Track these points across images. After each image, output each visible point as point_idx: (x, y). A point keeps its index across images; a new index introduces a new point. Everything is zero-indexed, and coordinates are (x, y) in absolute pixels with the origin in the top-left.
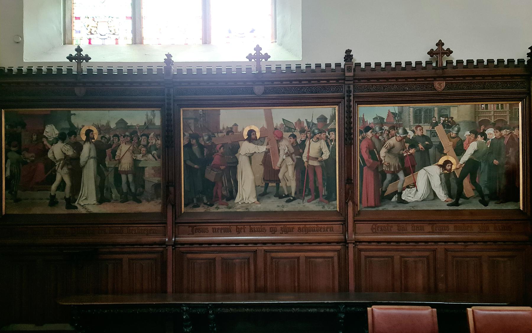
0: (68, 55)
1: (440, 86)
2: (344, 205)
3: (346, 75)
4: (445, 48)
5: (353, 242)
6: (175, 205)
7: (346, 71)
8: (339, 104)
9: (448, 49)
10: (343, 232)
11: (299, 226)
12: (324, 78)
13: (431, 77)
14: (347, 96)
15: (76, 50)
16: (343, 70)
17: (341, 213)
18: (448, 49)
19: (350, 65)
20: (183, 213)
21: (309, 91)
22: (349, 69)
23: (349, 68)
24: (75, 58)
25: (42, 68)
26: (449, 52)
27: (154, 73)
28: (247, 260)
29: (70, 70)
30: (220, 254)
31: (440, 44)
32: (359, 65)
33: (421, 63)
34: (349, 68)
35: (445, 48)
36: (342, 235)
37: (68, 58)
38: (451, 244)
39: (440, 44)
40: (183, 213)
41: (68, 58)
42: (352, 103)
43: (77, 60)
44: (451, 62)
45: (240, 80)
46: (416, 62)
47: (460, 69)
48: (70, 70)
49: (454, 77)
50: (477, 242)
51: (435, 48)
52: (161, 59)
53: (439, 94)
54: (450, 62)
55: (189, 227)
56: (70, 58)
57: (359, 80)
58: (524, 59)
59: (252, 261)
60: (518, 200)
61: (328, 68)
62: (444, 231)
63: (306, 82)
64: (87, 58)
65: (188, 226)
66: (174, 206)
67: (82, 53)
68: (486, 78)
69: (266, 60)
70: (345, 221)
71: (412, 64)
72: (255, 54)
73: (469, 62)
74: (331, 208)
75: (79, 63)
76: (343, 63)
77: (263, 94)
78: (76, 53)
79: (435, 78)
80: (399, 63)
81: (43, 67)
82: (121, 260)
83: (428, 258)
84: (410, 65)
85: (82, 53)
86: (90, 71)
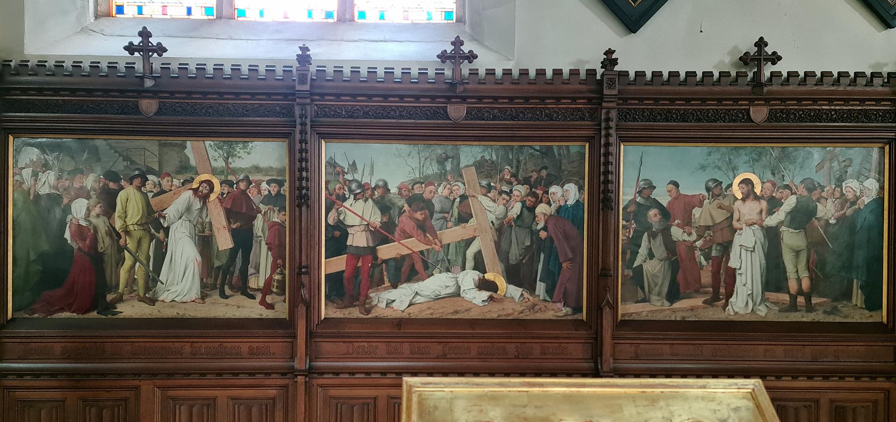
0: (127, 44)
1: (457, 111)
2: (596, 309)
3: (605, 93)
4: (769, 50)
5: (305, 373)
6: (310, 306)
7: (605, 85)
8: (892, 142)
9: (774, 53)
10: (592, 357)
11: (250, 344)
12: (711, 97)
13: (536, 98)
14: (300, 124)
15: (140, 34)
16: (601, 82)
17: (590, 324)
18: (774, 53)
19: (305, 72)
20: (322, 319)
21: (630, 115)
22: (303, 79)
23: (303, 77)
24: (138, 49)
25: (46, 64)
26: (775, 58)
27: (190, 76)
28: (272, 401)
29: (130, 67)
30: (199, 391)
31: (761, 44)
32: (626, 74)
33: (678, 75)
34: (303, 77)
35: (769, 50)
36: (592, 361)
37: (126, 48)
38: (391, 377)
39: (761, 44)
40: (9, 318)
41: (126, 48)
42: (612, 140)
43: (141, 53)
44: (660, 74)
45: (102, 88)
46: (703, 72)
47: (507, 85)
48: (130, 67)
49: (480, 99)
50: (57, 374)
51: (450, 48)
52: (289, 53)
53: (456, 126)
54: (474, 73)
55: (630, 346)
56: (130, 48)
57: (323, 95)
58: (831, 72)
59: (881, 408)
60: (881, 307)
61: (489, 77)
62: (168, 357)
63: (279, 97)
64: (161, 50)
65: (629, 345)
66: (308, 306)
67: (150, 39)
68: (771, 102)
69: (160, 55)
70: (597, 338)
71: (714, 75)
72: (452, 51)
73: (673, 76)
74: (878, 320)
75: (146, 58)
76: (600, 71)
77: (155, 114)
78: (140, 39)
79: (449, 99)
80: (559, 72)
81: (12, 61)
82: (215, 399)
83: (875, 403)
84: (711, 78)
85: (150, 39)
86: (165, 69)
